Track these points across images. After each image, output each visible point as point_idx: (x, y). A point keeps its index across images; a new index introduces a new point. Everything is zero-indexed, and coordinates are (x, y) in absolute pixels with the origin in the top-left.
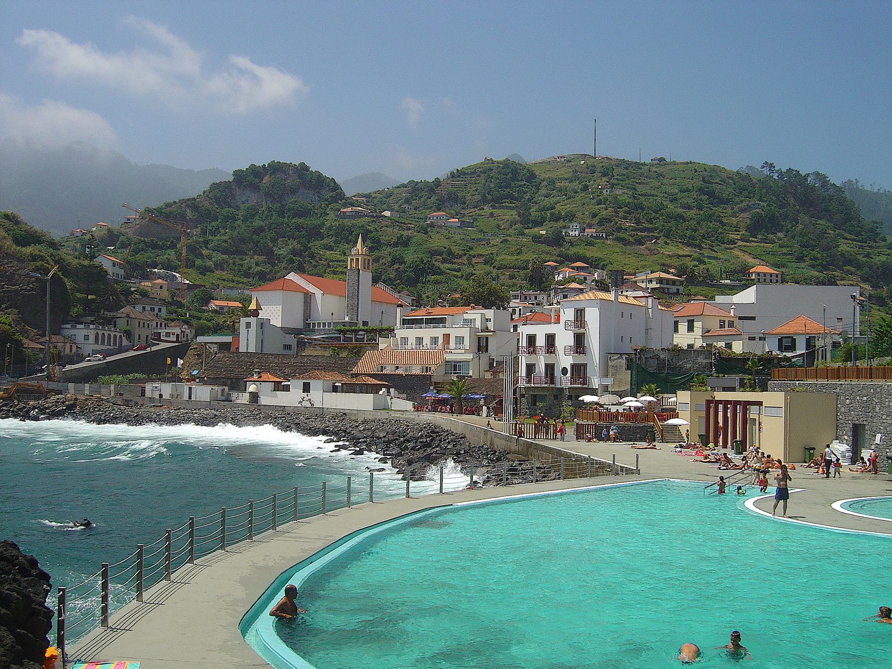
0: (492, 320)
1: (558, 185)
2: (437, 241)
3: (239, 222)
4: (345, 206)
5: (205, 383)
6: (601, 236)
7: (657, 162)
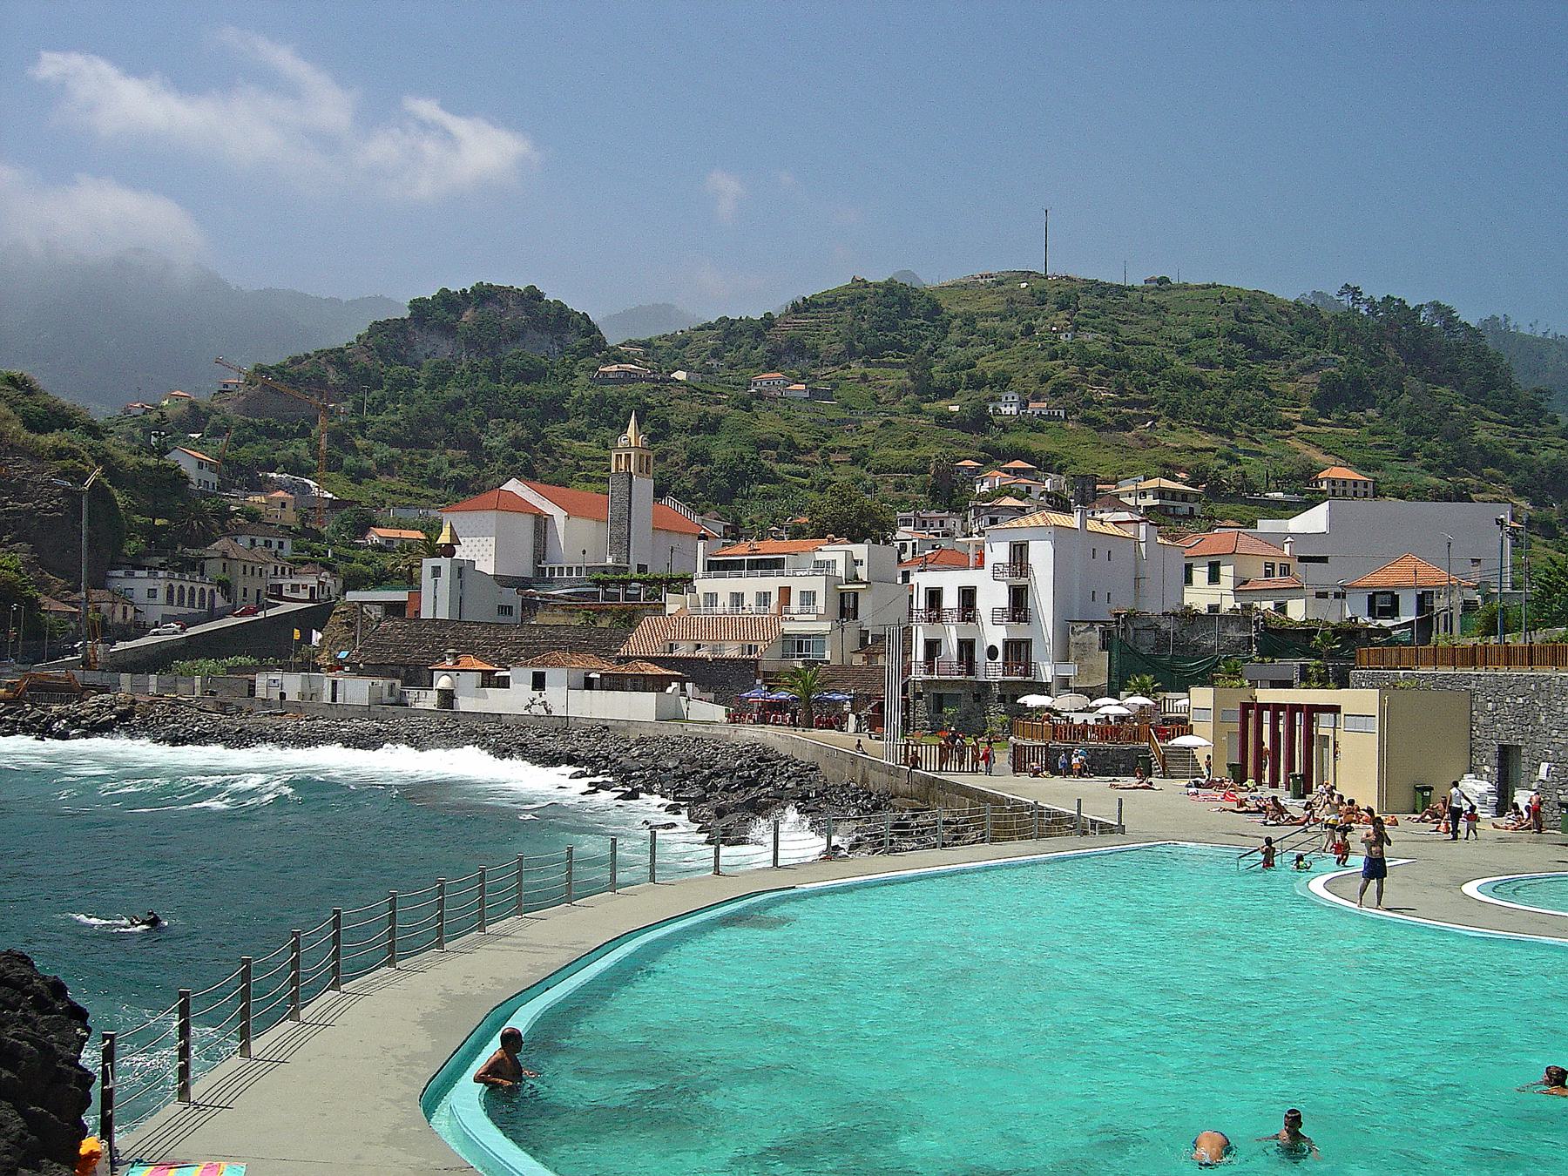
0: (865, 563)
1: (980, 325)
2: (768, 425)
3: (420, 391)
4: (606, 362)
5: (361, 673)
6: (1056, 414)
7: (1155, 284)
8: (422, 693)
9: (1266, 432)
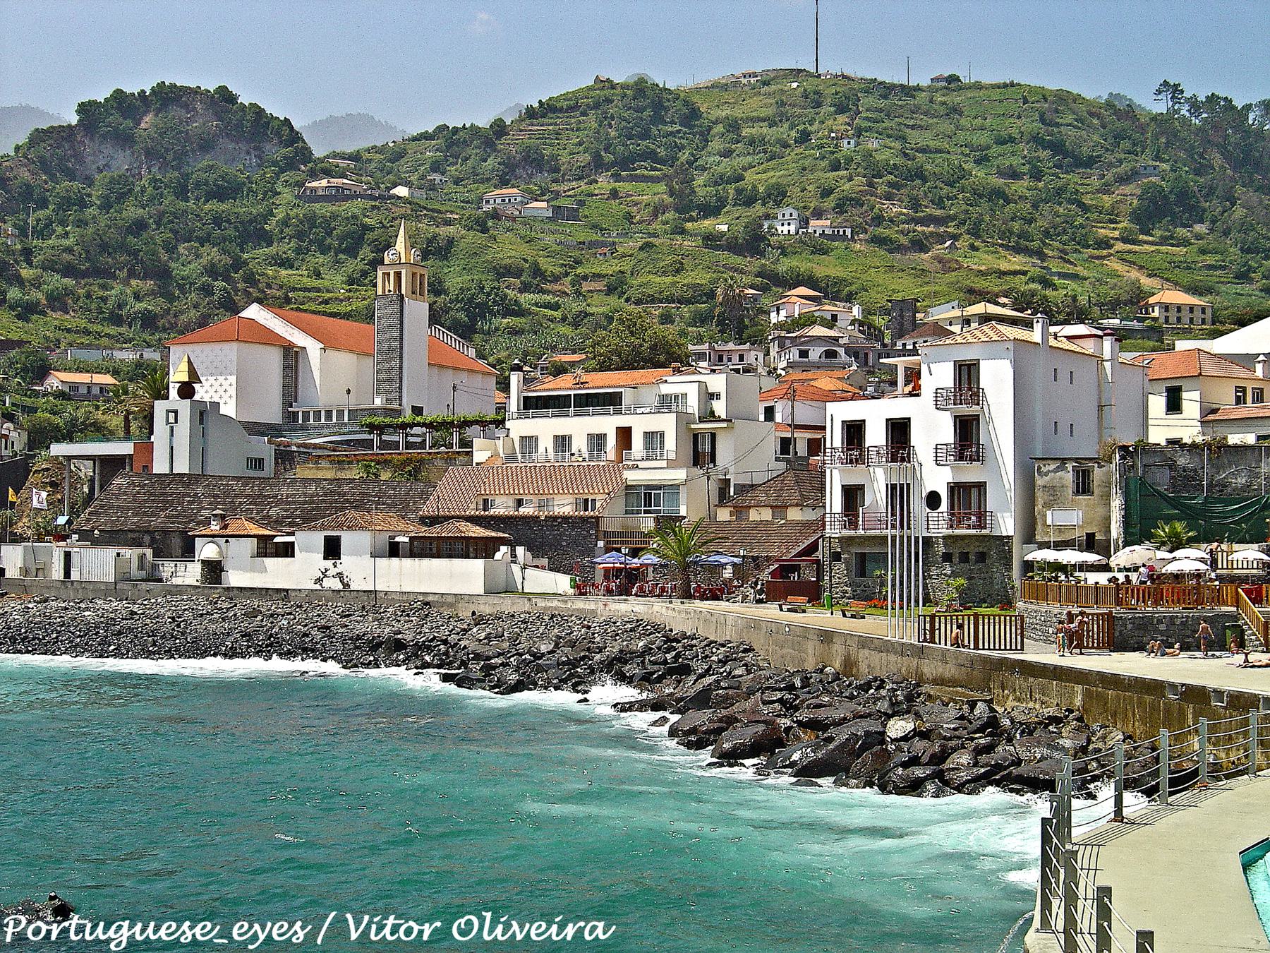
1: (746, 131)
2: (508, 248)
3: (93, 211)
4: (314, 175)
5: (96, 543)
6: (841, 233)
7: (944, 84)
8: (181, 566)
9: (1080, 252)
